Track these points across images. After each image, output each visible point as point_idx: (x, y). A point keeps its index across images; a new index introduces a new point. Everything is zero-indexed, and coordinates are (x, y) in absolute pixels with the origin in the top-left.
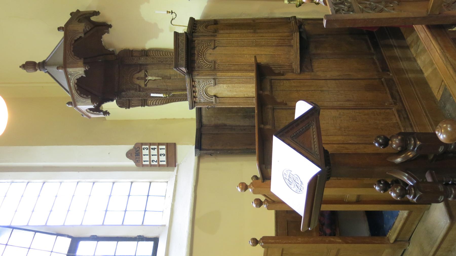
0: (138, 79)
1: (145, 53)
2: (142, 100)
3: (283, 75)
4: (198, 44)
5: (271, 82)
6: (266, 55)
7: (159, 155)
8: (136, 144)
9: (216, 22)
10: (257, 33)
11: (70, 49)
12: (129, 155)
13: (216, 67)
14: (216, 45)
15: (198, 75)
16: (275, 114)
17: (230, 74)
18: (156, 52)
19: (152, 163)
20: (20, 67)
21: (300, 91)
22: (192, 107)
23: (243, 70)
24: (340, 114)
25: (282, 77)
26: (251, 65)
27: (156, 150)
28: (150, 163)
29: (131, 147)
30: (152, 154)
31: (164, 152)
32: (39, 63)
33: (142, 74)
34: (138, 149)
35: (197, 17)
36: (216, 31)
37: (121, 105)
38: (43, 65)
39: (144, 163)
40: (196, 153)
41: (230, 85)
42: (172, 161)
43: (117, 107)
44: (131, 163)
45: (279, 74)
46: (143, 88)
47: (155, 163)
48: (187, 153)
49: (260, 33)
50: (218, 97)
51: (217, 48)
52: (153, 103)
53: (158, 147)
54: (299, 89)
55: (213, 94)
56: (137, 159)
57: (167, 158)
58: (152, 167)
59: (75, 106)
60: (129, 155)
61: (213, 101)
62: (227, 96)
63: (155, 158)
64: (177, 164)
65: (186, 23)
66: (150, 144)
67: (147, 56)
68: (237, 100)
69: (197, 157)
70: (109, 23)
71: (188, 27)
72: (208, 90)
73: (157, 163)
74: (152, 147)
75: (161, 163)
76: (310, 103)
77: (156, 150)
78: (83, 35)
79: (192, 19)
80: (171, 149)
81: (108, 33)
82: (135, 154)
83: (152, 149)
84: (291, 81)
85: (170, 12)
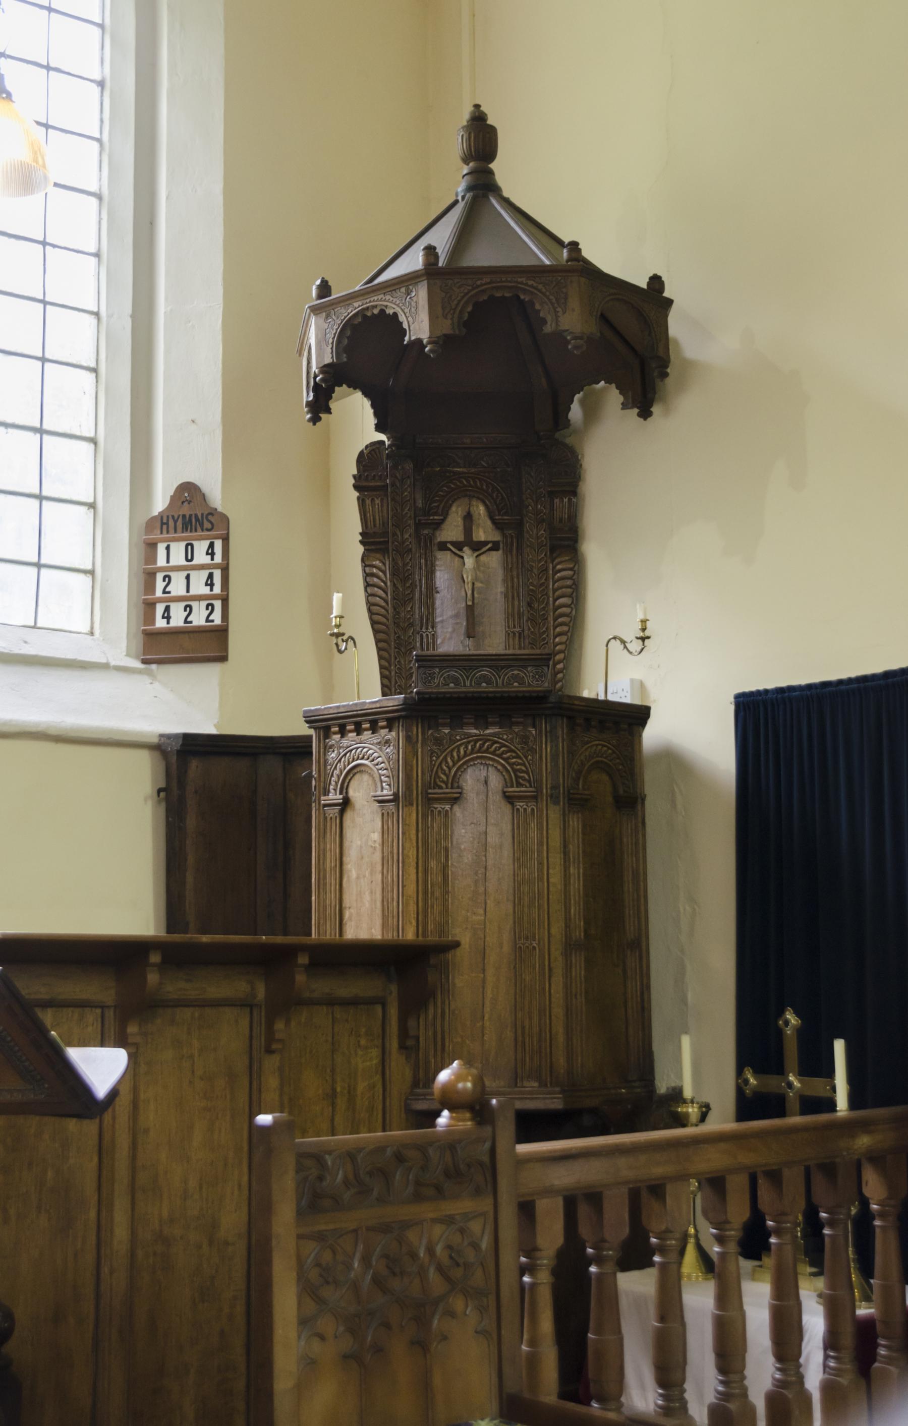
0: (468, 518)
1: (566, 541)
2: (385, 534)
3: (402, 1047)
4: (525, 740)
5: (370, 1002)
6: (481, 987)
7: (188, 602)
8: (225, 520)
9: (630, 801)
10: (567, 954)
11: (497, 288)
12: (188, 493)
13: (439, 806)
14: (519, 804)
15: (408, 738)
16: (227, 1010)
17: (412, 853)
18: (569, 582)
19: (160, 576)
20: (477, 106)
21: (333, 1105)
22: (311, 720)
23: (425, 900)
24: (227, 1243)
25: (394, 1044)
26: (442, 928)
27: (206, 590)
28: (161, 569)
29: (216, 497)
30: (193, 574)
31: (199, 619)
32: (491, 173)
33: (484, 532)
34: (207, 525)
35: (653, 735)
36: (576, 802)
37: (369, 459)
38: (483, 186)
39: (161, 548)
40: (169, 737)
41: (378, 856)
42: (170, 646)
43: (361, 447)
44: (160, 503)
45: (404, 1033)
46: (431, 538)
47: (160, 585)
48: (191, 704)
49: (568, 967)
50: (342, 812)
51: (509, 806)
52: (373, 575)
53: (215, 597)
54: (341, 1103)
55: (351, 793)
56: (171, 523)
57: (199, 631)
58: (142, 577)
59: (315, 310)
60: (188, 493)
61: (331, 796)
62: (346, 844)
63: (178, 587)
64: (154, 667)
65: (621, 693)
66: (225, 570)
67: (553, 549)
68: (331, 881)
69: (155, 740)
70: (655, 409)
71: (607, 702)
72: (366, 777)
73: (159, 593)
74: (217, 575)
75: (160, 609)
76: (114, 1094)
77: (206, 590)
78: (548, 329)
79: (638, 715)
80: (207, 645)
81: (625, 406)
82: (191, 515)
83: (211, 576)
84: (378, 1078)
85: (644, 630)
